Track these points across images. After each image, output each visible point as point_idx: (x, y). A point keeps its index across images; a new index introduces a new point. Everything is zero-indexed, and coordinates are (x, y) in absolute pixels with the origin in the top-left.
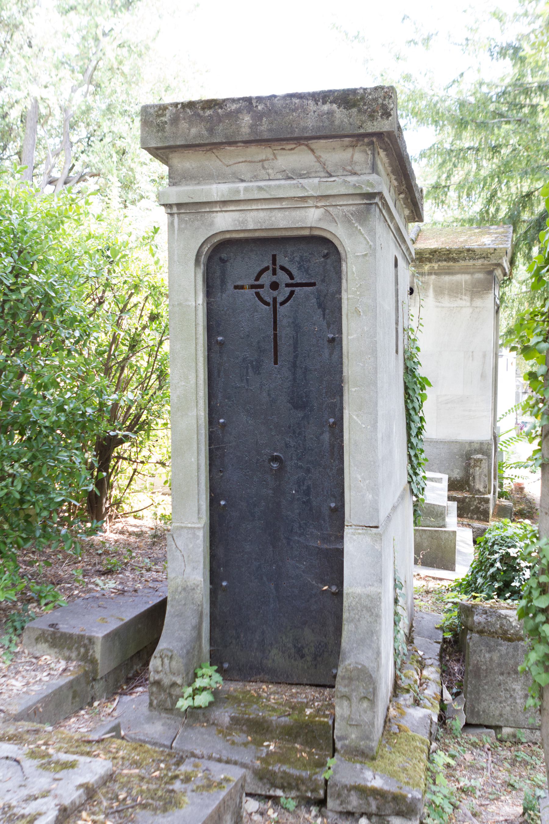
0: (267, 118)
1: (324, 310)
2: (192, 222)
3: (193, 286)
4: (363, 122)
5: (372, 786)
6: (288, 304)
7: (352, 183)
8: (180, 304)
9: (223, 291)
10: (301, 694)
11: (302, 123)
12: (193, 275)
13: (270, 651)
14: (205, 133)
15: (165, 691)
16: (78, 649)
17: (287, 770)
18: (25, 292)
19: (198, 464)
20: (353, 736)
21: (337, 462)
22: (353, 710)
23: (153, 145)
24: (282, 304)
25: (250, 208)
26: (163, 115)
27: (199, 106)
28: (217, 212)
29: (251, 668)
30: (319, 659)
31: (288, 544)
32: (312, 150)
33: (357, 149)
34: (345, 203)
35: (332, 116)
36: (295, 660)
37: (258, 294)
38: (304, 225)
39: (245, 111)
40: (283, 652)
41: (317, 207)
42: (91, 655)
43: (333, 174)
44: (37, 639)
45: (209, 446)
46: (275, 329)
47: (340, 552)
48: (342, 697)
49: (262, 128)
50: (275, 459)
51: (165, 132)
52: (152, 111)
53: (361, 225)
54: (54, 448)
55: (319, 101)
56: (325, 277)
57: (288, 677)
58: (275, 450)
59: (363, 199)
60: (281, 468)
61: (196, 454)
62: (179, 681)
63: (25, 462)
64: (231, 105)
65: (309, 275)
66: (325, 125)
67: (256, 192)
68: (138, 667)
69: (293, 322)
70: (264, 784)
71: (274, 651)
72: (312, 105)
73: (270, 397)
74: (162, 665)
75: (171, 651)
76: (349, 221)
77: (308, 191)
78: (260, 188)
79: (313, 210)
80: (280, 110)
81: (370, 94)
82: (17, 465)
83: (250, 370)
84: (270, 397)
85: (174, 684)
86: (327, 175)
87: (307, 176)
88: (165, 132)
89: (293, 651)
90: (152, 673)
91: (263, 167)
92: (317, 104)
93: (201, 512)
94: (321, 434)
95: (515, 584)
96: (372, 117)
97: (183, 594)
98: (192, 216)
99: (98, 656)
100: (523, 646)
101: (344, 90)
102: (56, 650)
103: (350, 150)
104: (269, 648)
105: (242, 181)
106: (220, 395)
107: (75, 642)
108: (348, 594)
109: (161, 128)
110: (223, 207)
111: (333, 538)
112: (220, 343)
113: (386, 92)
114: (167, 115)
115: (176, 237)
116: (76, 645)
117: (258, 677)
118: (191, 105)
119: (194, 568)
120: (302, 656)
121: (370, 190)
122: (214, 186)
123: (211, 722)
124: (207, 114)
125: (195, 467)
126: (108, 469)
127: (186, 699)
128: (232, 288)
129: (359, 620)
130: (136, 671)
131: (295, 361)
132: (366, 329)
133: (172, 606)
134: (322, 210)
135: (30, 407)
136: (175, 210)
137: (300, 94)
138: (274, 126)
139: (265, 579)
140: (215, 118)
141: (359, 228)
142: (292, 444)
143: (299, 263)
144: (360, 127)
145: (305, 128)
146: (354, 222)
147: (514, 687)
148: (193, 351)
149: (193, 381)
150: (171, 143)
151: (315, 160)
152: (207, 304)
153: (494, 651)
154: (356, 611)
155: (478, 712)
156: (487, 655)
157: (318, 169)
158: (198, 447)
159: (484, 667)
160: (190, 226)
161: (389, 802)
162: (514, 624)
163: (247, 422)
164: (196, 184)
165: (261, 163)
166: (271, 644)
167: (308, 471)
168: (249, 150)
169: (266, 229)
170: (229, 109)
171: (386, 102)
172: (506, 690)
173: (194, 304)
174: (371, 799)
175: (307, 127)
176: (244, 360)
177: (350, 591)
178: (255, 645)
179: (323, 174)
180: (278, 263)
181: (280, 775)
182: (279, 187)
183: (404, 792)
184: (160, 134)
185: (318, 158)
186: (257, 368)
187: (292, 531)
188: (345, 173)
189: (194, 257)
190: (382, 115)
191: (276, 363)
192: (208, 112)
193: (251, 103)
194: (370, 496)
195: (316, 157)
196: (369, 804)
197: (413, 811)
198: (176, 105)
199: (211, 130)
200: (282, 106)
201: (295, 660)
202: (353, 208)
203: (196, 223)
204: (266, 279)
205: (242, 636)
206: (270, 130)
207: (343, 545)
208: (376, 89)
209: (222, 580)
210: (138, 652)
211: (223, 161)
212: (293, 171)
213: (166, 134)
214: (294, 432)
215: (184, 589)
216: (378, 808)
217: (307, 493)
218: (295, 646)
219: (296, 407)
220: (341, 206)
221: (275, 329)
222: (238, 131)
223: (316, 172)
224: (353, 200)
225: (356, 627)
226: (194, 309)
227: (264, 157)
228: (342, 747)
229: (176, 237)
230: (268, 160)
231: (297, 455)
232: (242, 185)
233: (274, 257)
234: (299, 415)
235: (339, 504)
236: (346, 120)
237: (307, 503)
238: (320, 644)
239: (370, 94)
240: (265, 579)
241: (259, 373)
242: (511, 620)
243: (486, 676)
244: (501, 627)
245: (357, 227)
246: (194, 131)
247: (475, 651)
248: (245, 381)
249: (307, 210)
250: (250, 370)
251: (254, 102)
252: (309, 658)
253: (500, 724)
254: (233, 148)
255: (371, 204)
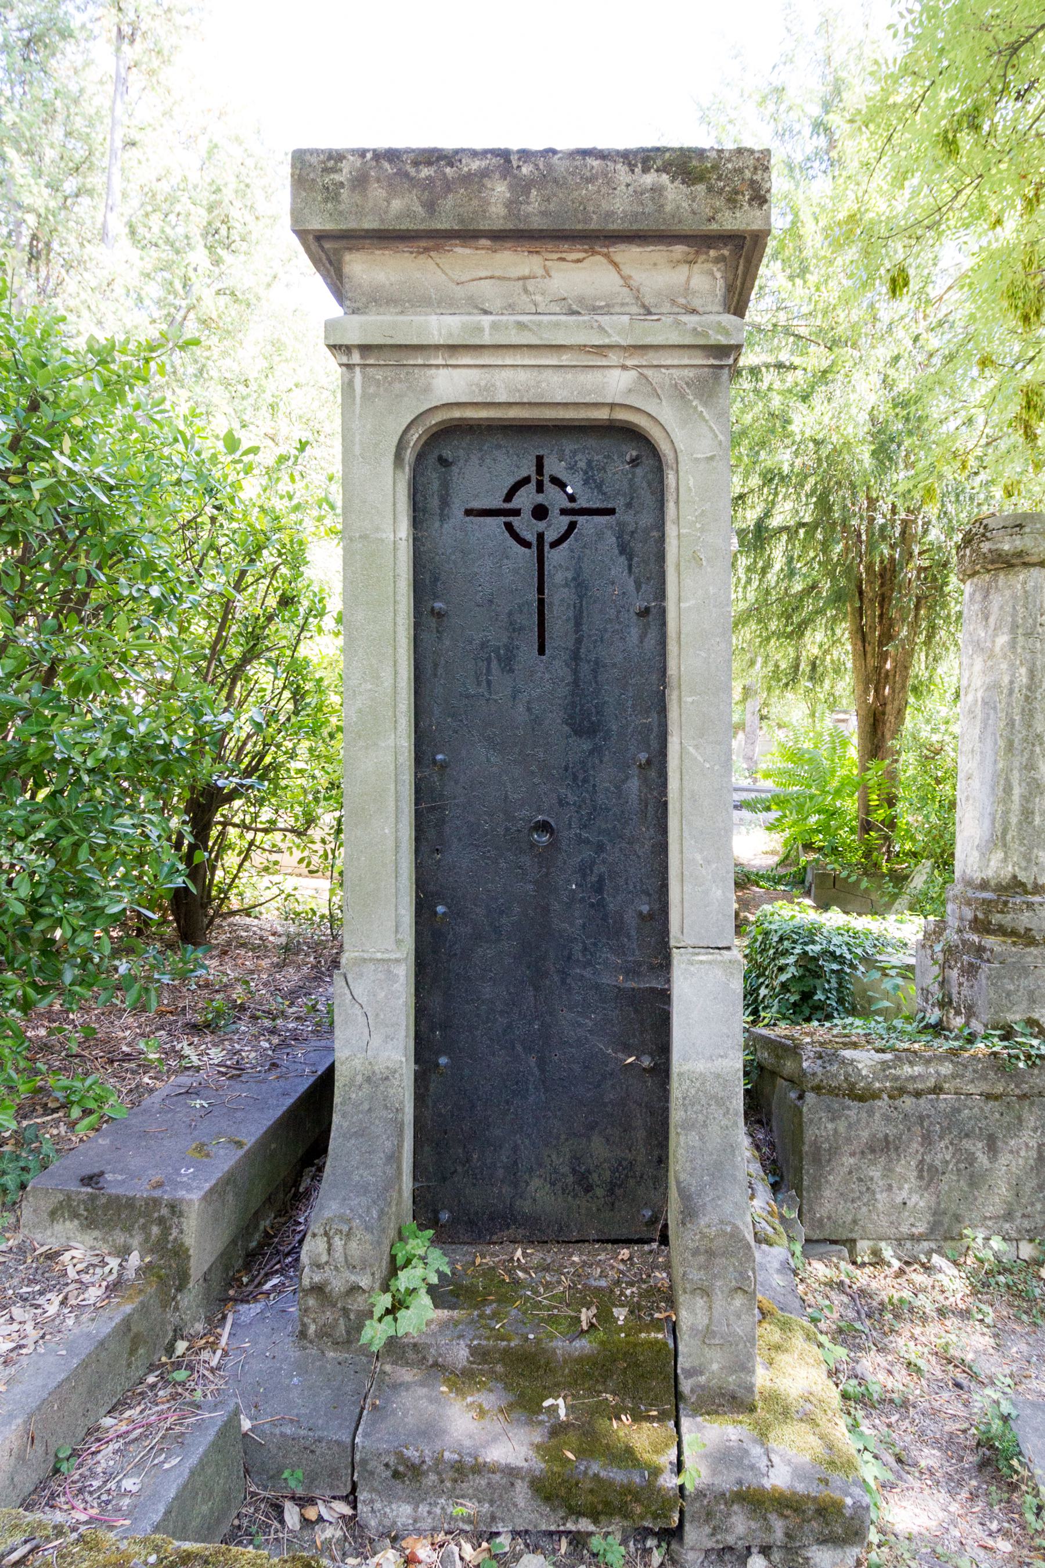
0: (538, 190)
1: (630, 559)
2: (390, 384)
3: (390, 504)
4: (717, 211)
5: (774, 1488)
6: (565, 545)
7: (690, 326)
8: (364, 537)
9: (443, 517)
10: (591, 1266)
11: (605, 206)
12: (391, 483)
13: (527, 1184)
14: (419, 210)
15: (334, 1306)
16: (144, 1228)
17: (603, 1474)
18: (41, 487)
19: (396, 838)
20: (715, 1367)
21: (652, 831)
22: (716, 1314)
23: (317, 224)
24: (554, 545)
25: (500, 363)
26: (335, 170)
27: (408, 158)
28: (437, 366)
29: (492, 1219)
30: (619, 1192)
31: (563, 982)
32: (615, 265)
33: (696, 268)
34: (676, 362)
35: (661, 195)
36: (575, 1197)
37: (509, 527)
38: (600, 400)
39: (497, 175)
40: (553, 1184)
41: (624, 367)
42: (175, 1239)
43: (653, 310)
44: (53, 1214)
45: (416, 804)
46: (541, 590)
47: (664, 996)
48: (693, 1291)
49: (530, 209)
50: (544, 827)
51: (339, 202)
52: (314, 160)
53: (705, 404)
54: (104, 811)
55: (636, 165)
56: (632, 499)
57: (560, 1230)
58: (539, 811)
59: (708, 357)
60: (553, 845)
61: (392, 820)
62: (364, 1282)
63: (40, 840)
64: (469, 161)
65: (604, 494)
66: (647, 210)
67: (513, 332)
68: (268, 1222)
69: (574, 579)
70: (553, 1510)
71: (536, 1183)
72: (623, 173)
73: (531, 714)
74: (329, 1250)
75: (349, 1221)
76: (683, 396)
77: (609, 336)
78: (521, 326)
79: (617, 372)
80: (564, 177)
81: (729, 160)
82: (19, 846)
83: (494, 664)
84: (531, 714)
85: (354, 1289)
86: (642, 311)
87: (607, 310)
88: (339, 202)
89: (570, 1179)
90: (306, 1270)
91: (526, 290)
92: (633, 171)
93: (401, 929)
94: (624, 781)
95: (819, 996)
96: (732, 202)
97: (366, 1089)
98: (389, 373)
99: (190, 1240)
100: (880, 1107)
101: (681, 149)
102: (96, 1233)
103: (685, 268)
104: (526, 1177)
105: (486, 312)
106: (436, 710)
107: (140, 1215)
108: (680, 1074)
109: (331, 194)
110: (450, 357)
111: (644, 969)
112: (439, 613)
113: (758, 159)
114: (345, 171)
115: (357, 412)
116: (142, 1221)
117: (506, 1233)
118: (392, 155)
119: (387, 1037)
120: (588, 1189)
121: (723, 340)
122: (433, 319)
123: (431, 1362)
124: (422, 175)
125: (391, 843)
126: (207, 841)
127: (380, 1320)
128: (460, 513)
129: (705, 1125)
130: (266, 1232)
131: (578, 649)
132: (712, 590)
133: (344, 1116)
134: (633, 373)
135: (53, 727)
136: (356, 358)
137: (601, 151)
138: (552, 207)
139: (519, 1048)
140: (438, 183)
141: (700, 408)
142: (572, 799)
143: (586, 473)
144: (710, 220)
145: (610, 215)
146: (691, 397)
147: (871, 1174)
148: (389, 626)
149: (388, 683)
150: (352, 224)
151: (622, 282)
152: (414, 539)
153: (839, 1117)
154: (697, 1107)
155: (821, 1220)
156: (830, 1126)
157: (627, 300)
158: (397, 807)
159: (826, 1146)
160: (386, 390)
161: (809, 1521)
162: (864, 1073)
163: (488, 760)
164: (397, 314)
165: (521, 282)
166: (531, 1170)
167: (600, 848)
168: (498, 256)
169: (530, 404)
170: (466, 169)
171: (757, 178)
172: (860, 1180)
173: (392, 536)
174: (773, 1517)
175: (613, 213)
176: (483, 645)
177: (685, 1068)
178: (500, 1173)
179: (635, 309)
180: (547, 471)
181: (587, 1485)
182: (557, 325)
183: (837, 1495)
184: (329, 205)
185: (626, 279)
186: (508, 661)
187: (569, 958)
188: (677, 310)
189: (394, 450)
190: (751, 199)
191: (542, 651)
192: (426, 172)
193: (508, 161)
194: (719, 893)
195: (622, 277)
196: (769, 1529)
197: (856, 1534)
198: (362, 153)
199: (431, 207)
200: (567, 170)
201: (575, 1197)
202: (689, 373)
203: (397, 386)
204: (525, 499)
205: (475, 1156)
206: (544, 214)
207: (668, 981)
208: (740, 151)
209: (439, 1053)
210: (269, 1199)
211: (450, 273)
212: (581, 300)
213: (342, 207)
214: (575, 778)
215: (368, 1080)
216: (787, 1535)
217: (599, 887)
218: (574, 1171)
219: (578, 732)
220: (667, 367)
221: (541, 590)
222: (484, 211)
223: (623, 304)
224: (690, 358)
225: (702, 1139)
226: (391, 547)
227: (527, 273)
228: (692, 1391)
229: (357, 412)
230: (534, 277)
231: (580, 820)
232: (486, 320)
233: (540, 462)
234: (585, 747)
235: (657, 906)
236: (685, 205)
237: (601, 905)
238: (620, 1164)
239: (729, 160)
240: (519, 1048)
241: (512, 671)
242: (860, 1066)
243: (830, 1160)
244: (846, 1079)
245: (696, 408)
246: (397, 205)
247: (811, 1121)
248: (484, 684)
249: (607, 372)
250: (494, 664)
251: (514, 159)
252: (599, 1192)
253: (854, 1236)
254: (468, 251)
255: (721, 367)
